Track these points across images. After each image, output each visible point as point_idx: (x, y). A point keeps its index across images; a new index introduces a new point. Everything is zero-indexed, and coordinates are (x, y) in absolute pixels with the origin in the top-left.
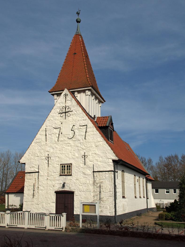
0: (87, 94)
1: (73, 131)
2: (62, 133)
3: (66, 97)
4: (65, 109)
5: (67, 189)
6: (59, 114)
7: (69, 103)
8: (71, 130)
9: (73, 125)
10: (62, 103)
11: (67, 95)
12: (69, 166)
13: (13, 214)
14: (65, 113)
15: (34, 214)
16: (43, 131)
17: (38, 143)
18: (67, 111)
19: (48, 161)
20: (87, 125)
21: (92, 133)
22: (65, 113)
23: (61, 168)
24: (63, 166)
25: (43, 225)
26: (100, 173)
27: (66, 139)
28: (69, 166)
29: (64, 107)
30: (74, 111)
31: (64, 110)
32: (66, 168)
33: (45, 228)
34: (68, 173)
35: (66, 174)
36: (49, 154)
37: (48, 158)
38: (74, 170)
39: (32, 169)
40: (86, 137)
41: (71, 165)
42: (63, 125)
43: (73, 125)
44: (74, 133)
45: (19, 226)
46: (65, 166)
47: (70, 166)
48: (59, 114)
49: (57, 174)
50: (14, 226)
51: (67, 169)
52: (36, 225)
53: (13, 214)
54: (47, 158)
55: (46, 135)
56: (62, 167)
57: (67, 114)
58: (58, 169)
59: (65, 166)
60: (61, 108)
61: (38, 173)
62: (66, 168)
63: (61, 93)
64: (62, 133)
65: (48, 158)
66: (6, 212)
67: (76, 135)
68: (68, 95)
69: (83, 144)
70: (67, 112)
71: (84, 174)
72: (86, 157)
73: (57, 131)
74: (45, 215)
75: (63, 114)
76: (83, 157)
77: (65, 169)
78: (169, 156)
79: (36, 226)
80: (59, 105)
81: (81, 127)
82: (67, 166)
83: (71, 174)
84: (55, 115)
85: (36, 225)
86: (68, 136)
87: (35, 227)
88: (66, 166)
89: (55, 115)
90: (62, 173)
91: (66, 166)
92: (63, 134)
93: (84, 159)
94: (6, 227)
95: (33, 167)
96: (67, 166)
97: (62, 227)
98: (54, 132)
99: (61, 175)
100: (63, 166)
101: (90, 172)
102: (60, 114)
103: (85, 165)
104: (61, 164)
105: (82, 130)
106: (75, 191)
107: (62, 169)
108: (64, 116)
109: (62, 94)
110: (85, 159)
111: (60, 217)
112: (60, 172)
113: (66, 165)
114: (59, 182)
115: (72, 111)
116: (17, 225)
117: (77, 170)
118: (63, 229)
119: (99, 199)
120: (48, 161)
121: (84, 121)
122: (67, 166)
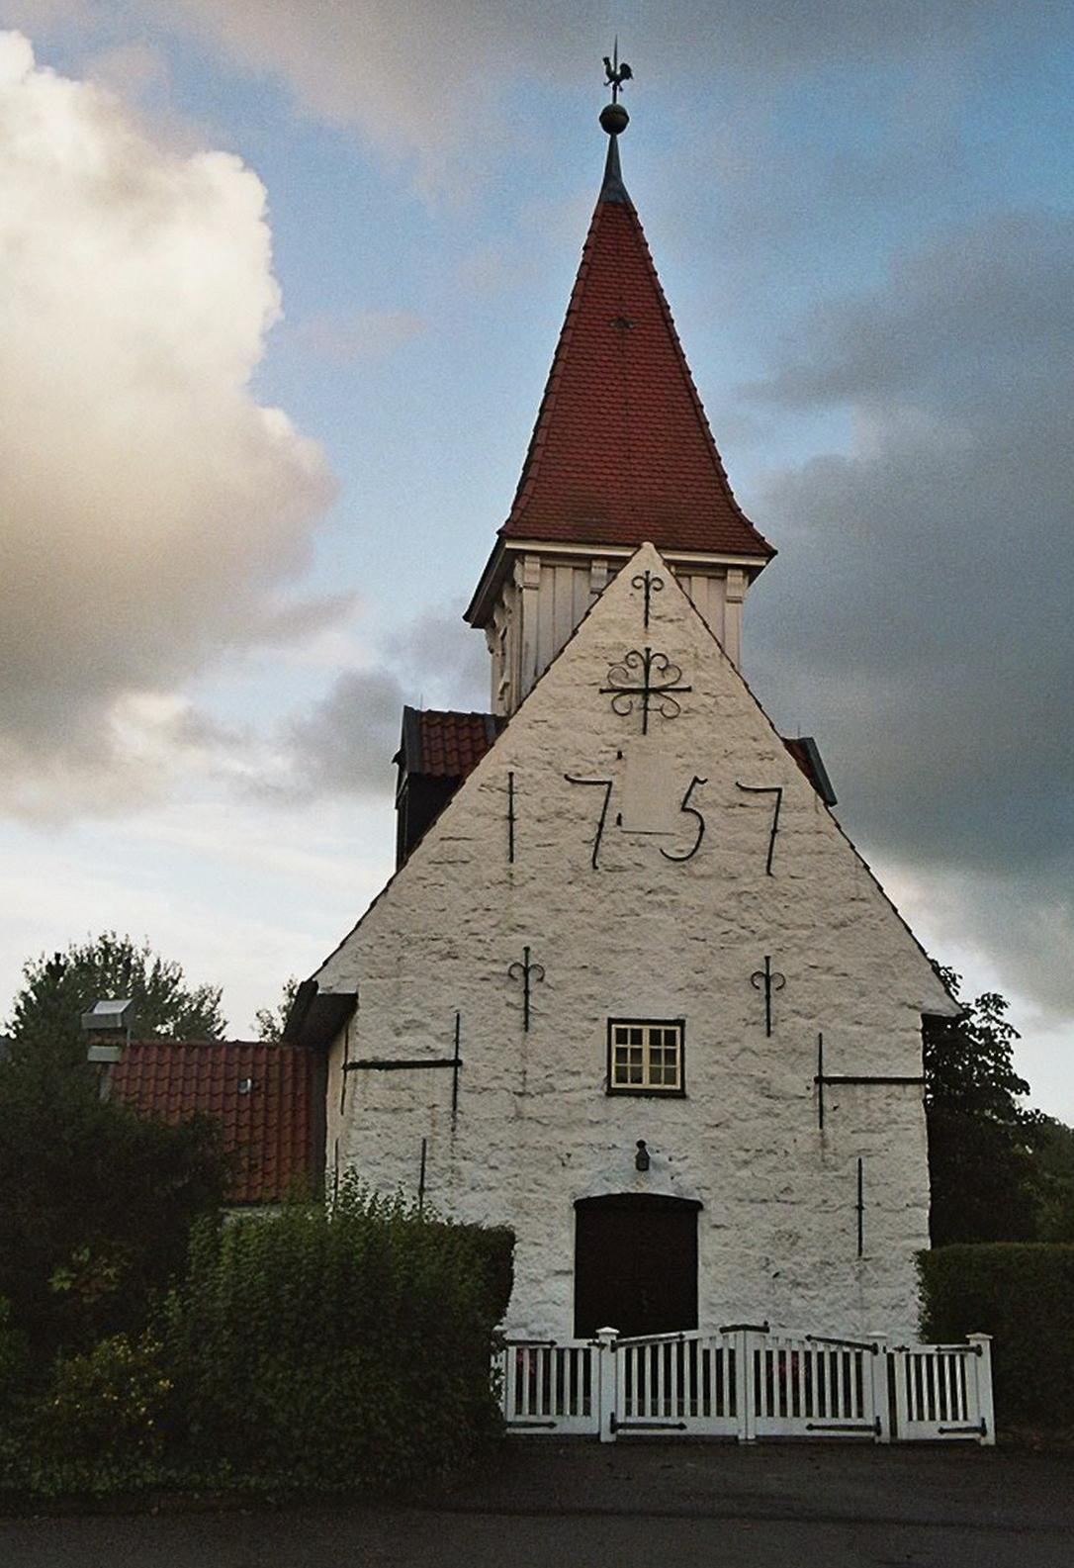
0: (731, 593)
1: (691, 817)
2: (620, 817)
3: (647, 597)
4: (642, 668)
5: (659, 1185)
6: (602, 691)
7: (664, 640)
8: (684, 809)
9: (696, 780)
10: (626, 628)
11: (657, 584)
12: (668, 1035)
13: (648, 1351)
14: (646, 692)
15: (561, 1352)
16: (488, 787)
17: (450, 868)
18: (656, 681)
19: (527, 992)
20: (779, 790)
21: (811, 841)
22: (646, 692)
23: (678, 1047)
24: (624, 1034)
25: (961, 1417)
26: (860, 1090)
27: (654, 863)
28: (668, 1035)
29: (634, 652)
30: (698, 690)
31: (637, 674)
32: (646, 1045)
33: (872, 1434)
34: (625, 1081)
35: (646, 1084)
36: (533, 949)
37: (526, 971)
38: (697, 1059)
39: (406, 1040)
40: (775, 864)
41: (678, 1028)
42: (625, 766)
43: (696, 780)
44: (702, 829)
45: (698, 1425)
46: (637, 1037)
47: (670, 1038)
48: (602, 691)
49: (591, 1081)
50: (850, 1428)
51: (655, 1055)
52: (944, 1418)
53: (648, 1351)
54: (517, 972)
55: (511, 818)
56: (621, 1036)
57: (654, 702)
58: (594, 1052)
59: (640, 1031)
60: (618, 657)
61: (451, 1070)
62: (646, 1045)
63: (625, 560)
64: (620, 817)
65: (526, 971)
66: (597, 1336)
67: (710, 840)
68: (662, 583)
69: (752, 903)
70: (658, 691)
71: (766, 1091)
72: (774, 985)
73: (588, 801)
74: (867, 1347)
75: (626, 699)
76: (760, 982)
77: (637, 1054)
78: (26, 987)
79: (945, 1425)
80: (606, 640)
81: (745, 798)
82: (651, 1030)
83: (678, 1087)
84: (575, 694)
85: (944, 1418)
86: (663, 842)
87: (942, 1431)
88: (646, 1038)
89: (575, 694)
90: (621, 1079)
91: (646, 1038)
92: (626, 825)
93: (763, 997)
94: (603, 1439)
95: (412, 1025)
96: (655, 1037)
97: (977, 1423)
98: (567, 806)
99: (612, 1093)
100: (624, 1034)
101: (799, 1081)
102: (612, 696)
103: (820, 1035)
104: (611, 1021)
105: (752, 813)
106: (706, 1195)
107: (621, 1053)
108: (637, 714)
109: (627, 573)
110: (768, 997)
111: (958, 1359)
112: (605, 1074)
113: (646, 1030)
114: (601, 1139)
115: (689, 690)
116: (683, 1420)
117: (717, 1062)
118: (983, 1430)
119: (857, 1252)
120: (768, 997)
121: (758, 764)
122: (651, 1030)
